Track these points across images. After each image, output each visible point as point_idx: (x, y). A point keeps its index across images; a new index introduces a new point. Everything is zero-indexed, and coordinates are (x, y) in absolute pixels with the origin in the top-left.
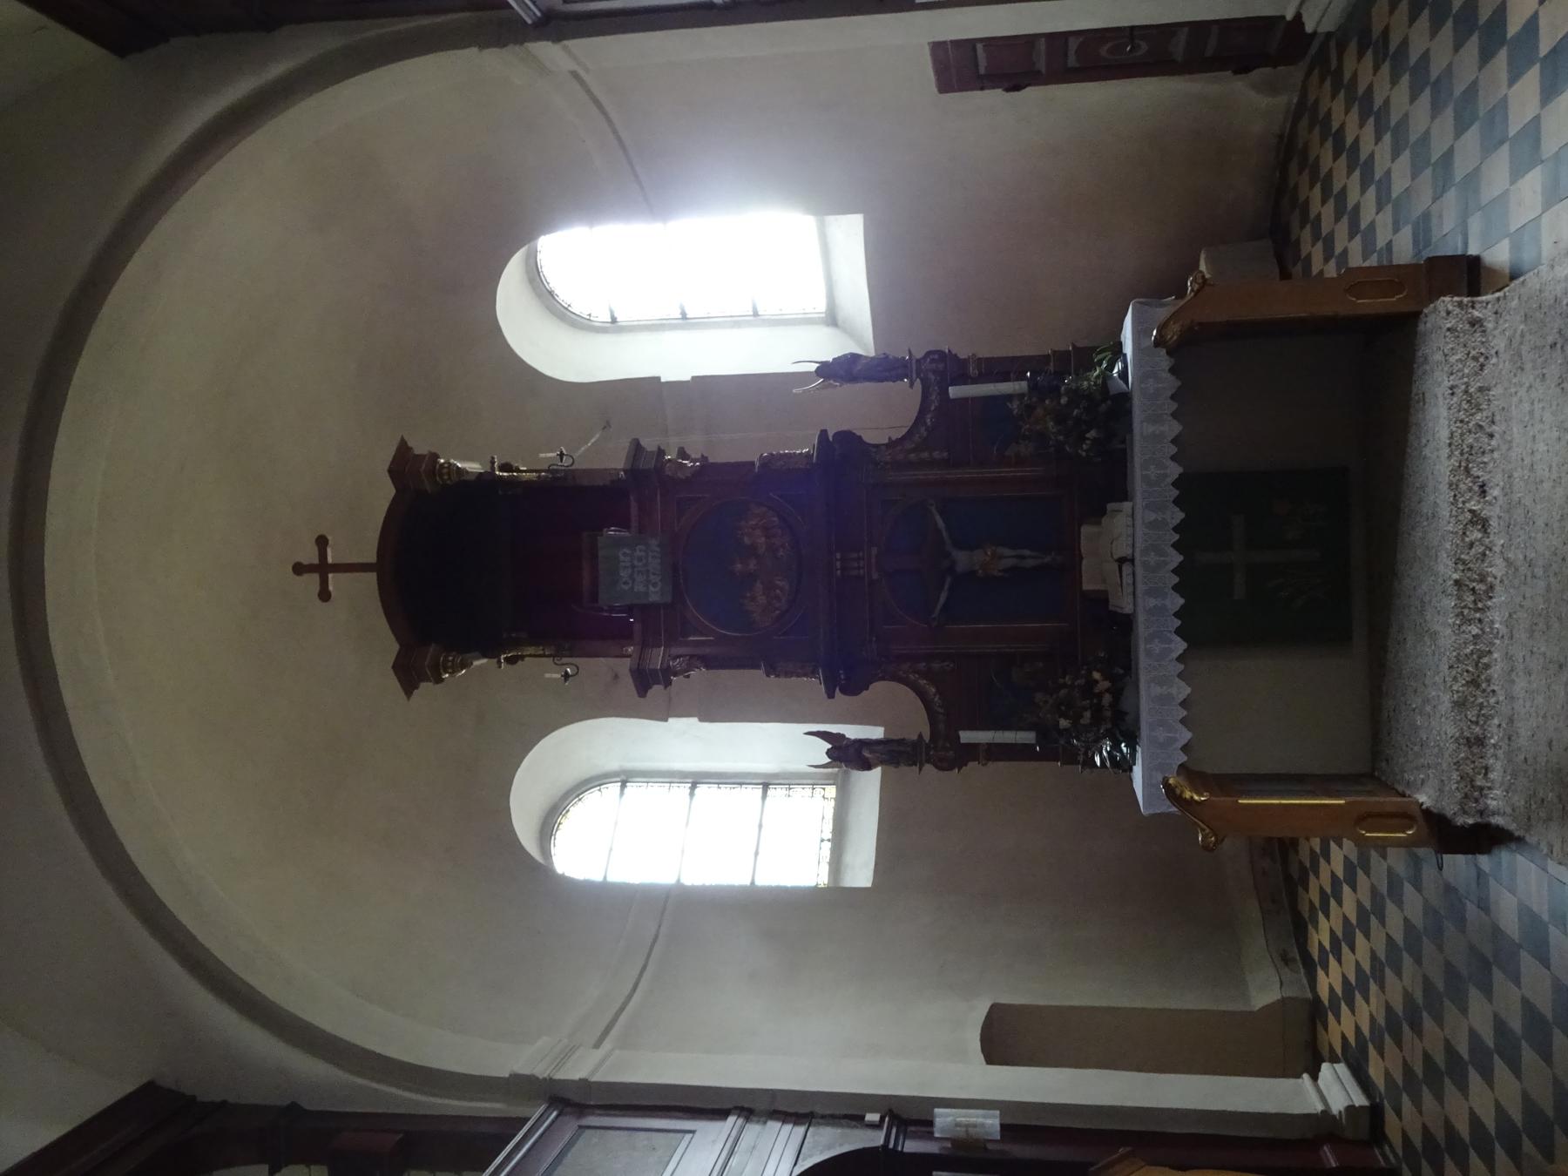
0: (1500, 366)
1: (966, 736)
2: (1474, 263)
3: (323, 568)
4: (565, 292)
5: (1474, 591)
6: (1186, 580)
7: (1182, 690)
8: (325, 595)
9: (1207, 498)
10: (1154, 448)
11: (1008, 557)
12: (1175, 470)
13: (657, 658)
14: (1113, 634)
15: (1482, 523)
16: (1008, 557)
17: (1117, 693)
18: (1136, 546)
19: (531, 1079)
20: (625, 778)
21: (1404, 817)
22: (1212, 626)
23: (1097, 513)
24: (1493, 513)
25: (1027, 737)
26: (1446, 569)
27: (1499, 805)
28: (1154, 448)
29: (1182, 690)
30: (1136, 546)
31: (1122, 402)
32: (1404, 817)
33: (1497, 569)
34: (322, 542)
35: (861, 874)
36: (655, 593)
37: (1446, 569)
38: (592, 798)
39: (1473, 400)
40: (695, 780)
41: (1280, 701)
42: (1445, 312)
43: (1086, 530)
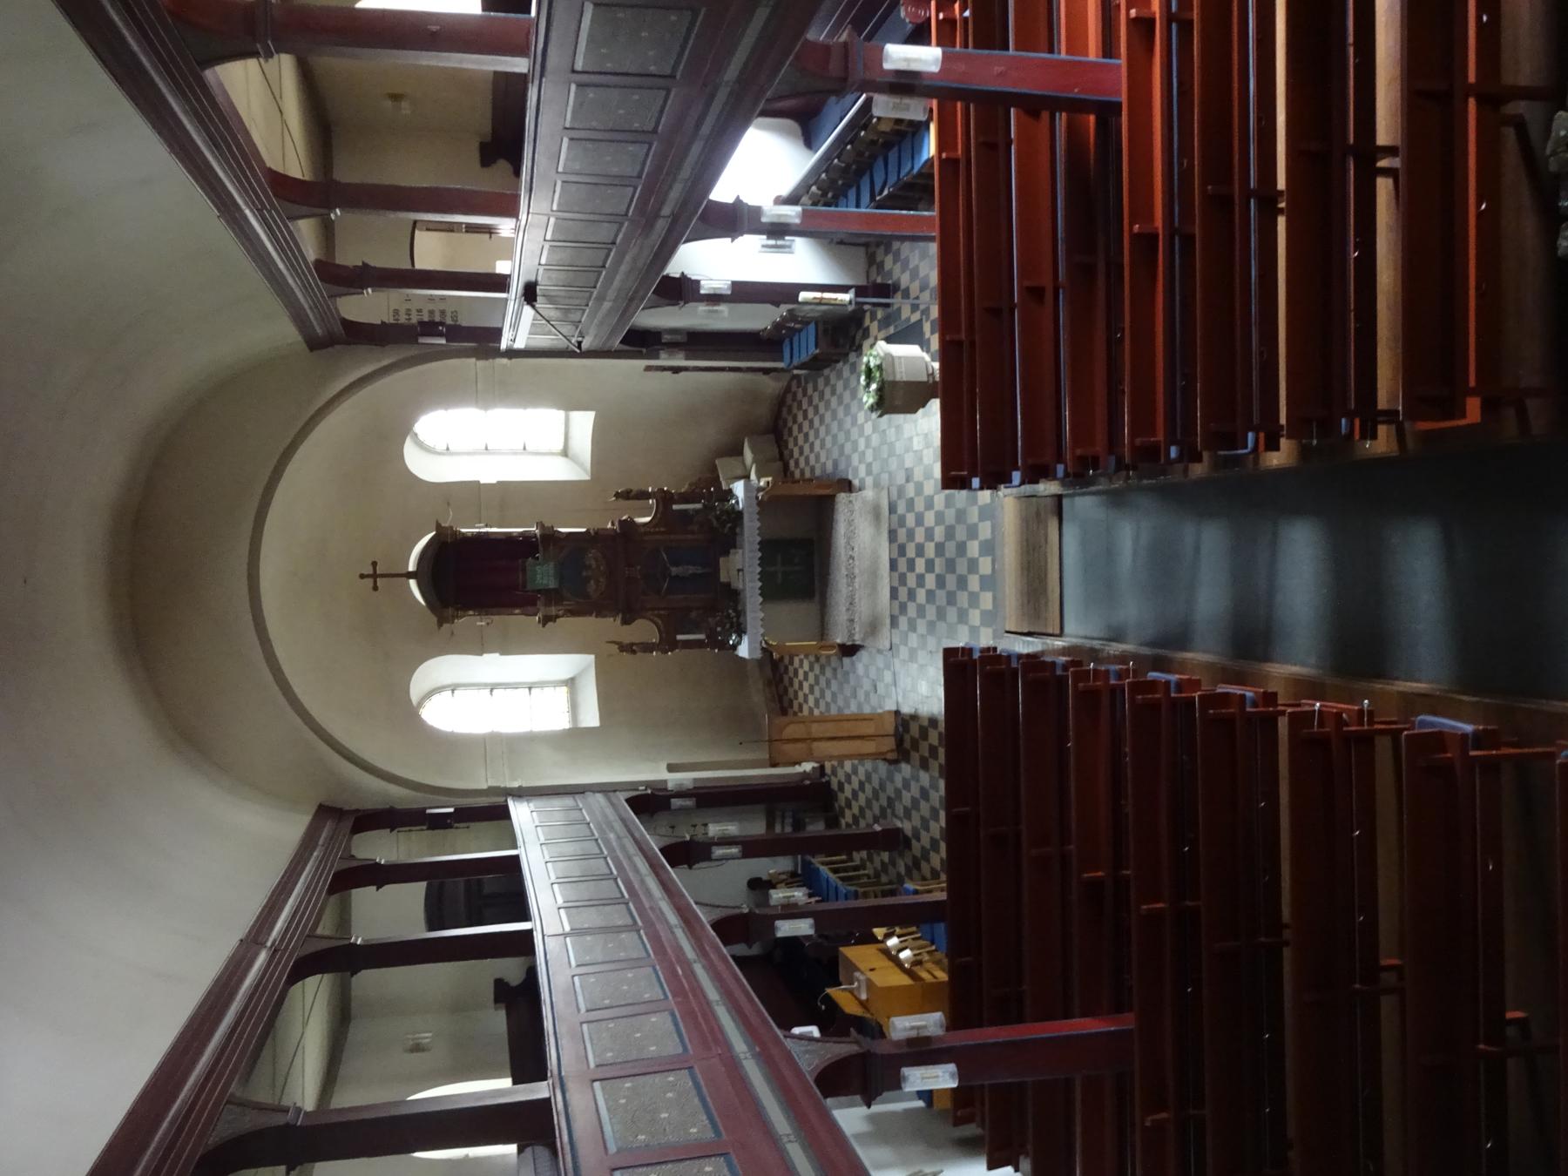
0: (856, 514)
1: (679, 637)
2: (850, 482)
3: (375, 576)
4: (429, 442)
5: (851, 577)
6: (763, 576)
7: (762, 615)
8: (375, 588)
9: (769, 548)
10: (751, 531)
11: (691, 570)
12: (759, 539)
13: (553, 611)
14: (733, 596)
15: (852, 558)
16: (691, 570)
17: (738, 617)
18: (744, 567)
19: (498, 788)
20: (454, 688)
21: (832, 647)
22: (772, 592)
23: (727, 553)
24: (856, 555)
25: (702, 637)
26: (844, 572)
27: (858, 639)
28: (751, 531)
29: (762, 615)
30: (744, 567)
31: (740, 514)
32: (832, 647)
33: (857, 571)
34: (374, 564)
35: (591, 717)
36: (552, 584)
37: (844, 572)
38: (436, 698)
39: (850, 523)
40: (492, 687)
41: (793, 613)
42: (842, 497)
43: (722, 560)
